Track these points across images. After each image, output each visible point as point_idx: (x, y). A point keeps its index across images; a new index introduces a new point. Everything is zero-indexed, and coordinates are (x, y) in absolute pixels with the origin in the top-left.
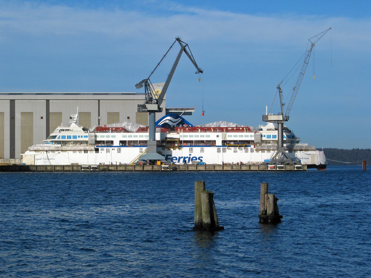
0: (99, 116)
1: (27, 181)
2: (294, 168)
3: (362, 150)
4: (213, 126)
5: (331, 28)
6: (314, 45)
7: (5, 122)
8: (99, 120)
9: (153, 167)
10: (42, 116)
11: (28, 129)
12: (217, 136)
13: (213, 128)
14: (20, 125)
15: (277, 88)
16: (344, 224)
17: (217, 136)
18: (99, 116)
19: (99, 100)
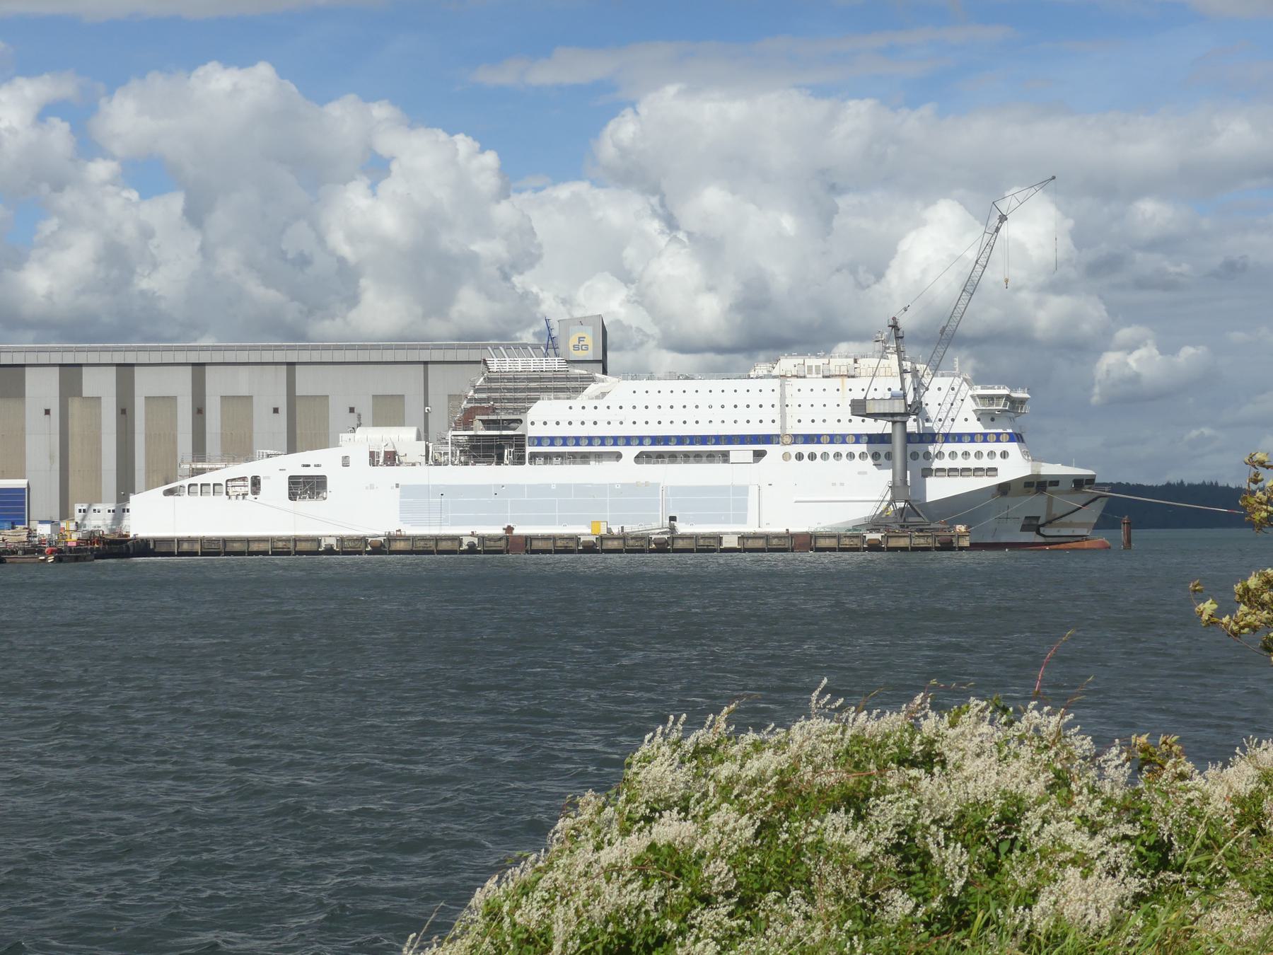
0: (426, 404)
1: (420, 569)
2: (649, 545)
3: (1191, 486)
4: (942, 431)
5: (1054, 178)
6: (1006, 219)
7: (180, 423)
8: (426, 415)
9: (193, 546)
10: (352, 406)
11: (163, 439)
12: (394, 453)
13: (944, 434)
14: (219, 431)
15: (890, 326)
16: (258, 760)
17: (394, 453)
18: (426, 404)
19: (199, 366)
